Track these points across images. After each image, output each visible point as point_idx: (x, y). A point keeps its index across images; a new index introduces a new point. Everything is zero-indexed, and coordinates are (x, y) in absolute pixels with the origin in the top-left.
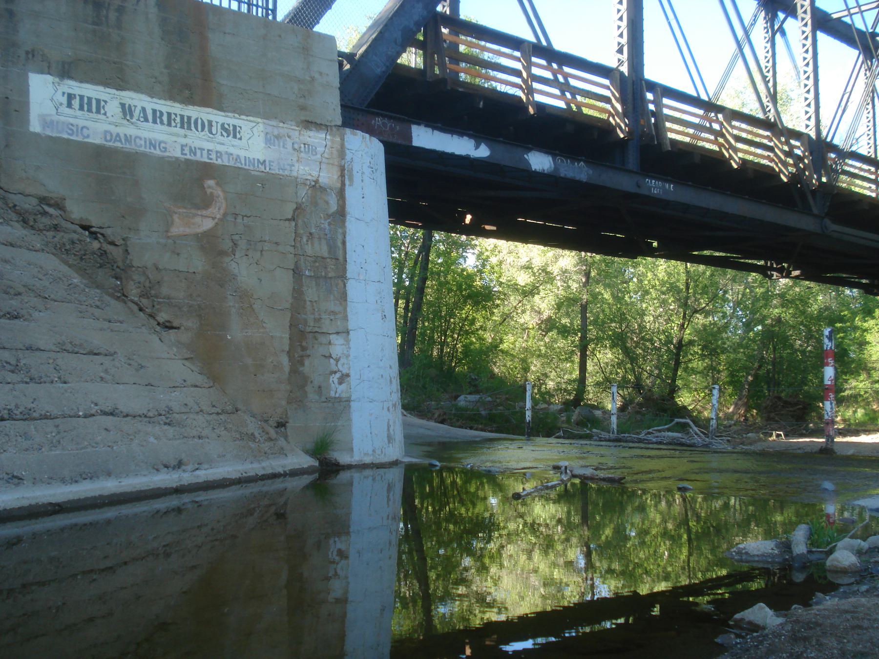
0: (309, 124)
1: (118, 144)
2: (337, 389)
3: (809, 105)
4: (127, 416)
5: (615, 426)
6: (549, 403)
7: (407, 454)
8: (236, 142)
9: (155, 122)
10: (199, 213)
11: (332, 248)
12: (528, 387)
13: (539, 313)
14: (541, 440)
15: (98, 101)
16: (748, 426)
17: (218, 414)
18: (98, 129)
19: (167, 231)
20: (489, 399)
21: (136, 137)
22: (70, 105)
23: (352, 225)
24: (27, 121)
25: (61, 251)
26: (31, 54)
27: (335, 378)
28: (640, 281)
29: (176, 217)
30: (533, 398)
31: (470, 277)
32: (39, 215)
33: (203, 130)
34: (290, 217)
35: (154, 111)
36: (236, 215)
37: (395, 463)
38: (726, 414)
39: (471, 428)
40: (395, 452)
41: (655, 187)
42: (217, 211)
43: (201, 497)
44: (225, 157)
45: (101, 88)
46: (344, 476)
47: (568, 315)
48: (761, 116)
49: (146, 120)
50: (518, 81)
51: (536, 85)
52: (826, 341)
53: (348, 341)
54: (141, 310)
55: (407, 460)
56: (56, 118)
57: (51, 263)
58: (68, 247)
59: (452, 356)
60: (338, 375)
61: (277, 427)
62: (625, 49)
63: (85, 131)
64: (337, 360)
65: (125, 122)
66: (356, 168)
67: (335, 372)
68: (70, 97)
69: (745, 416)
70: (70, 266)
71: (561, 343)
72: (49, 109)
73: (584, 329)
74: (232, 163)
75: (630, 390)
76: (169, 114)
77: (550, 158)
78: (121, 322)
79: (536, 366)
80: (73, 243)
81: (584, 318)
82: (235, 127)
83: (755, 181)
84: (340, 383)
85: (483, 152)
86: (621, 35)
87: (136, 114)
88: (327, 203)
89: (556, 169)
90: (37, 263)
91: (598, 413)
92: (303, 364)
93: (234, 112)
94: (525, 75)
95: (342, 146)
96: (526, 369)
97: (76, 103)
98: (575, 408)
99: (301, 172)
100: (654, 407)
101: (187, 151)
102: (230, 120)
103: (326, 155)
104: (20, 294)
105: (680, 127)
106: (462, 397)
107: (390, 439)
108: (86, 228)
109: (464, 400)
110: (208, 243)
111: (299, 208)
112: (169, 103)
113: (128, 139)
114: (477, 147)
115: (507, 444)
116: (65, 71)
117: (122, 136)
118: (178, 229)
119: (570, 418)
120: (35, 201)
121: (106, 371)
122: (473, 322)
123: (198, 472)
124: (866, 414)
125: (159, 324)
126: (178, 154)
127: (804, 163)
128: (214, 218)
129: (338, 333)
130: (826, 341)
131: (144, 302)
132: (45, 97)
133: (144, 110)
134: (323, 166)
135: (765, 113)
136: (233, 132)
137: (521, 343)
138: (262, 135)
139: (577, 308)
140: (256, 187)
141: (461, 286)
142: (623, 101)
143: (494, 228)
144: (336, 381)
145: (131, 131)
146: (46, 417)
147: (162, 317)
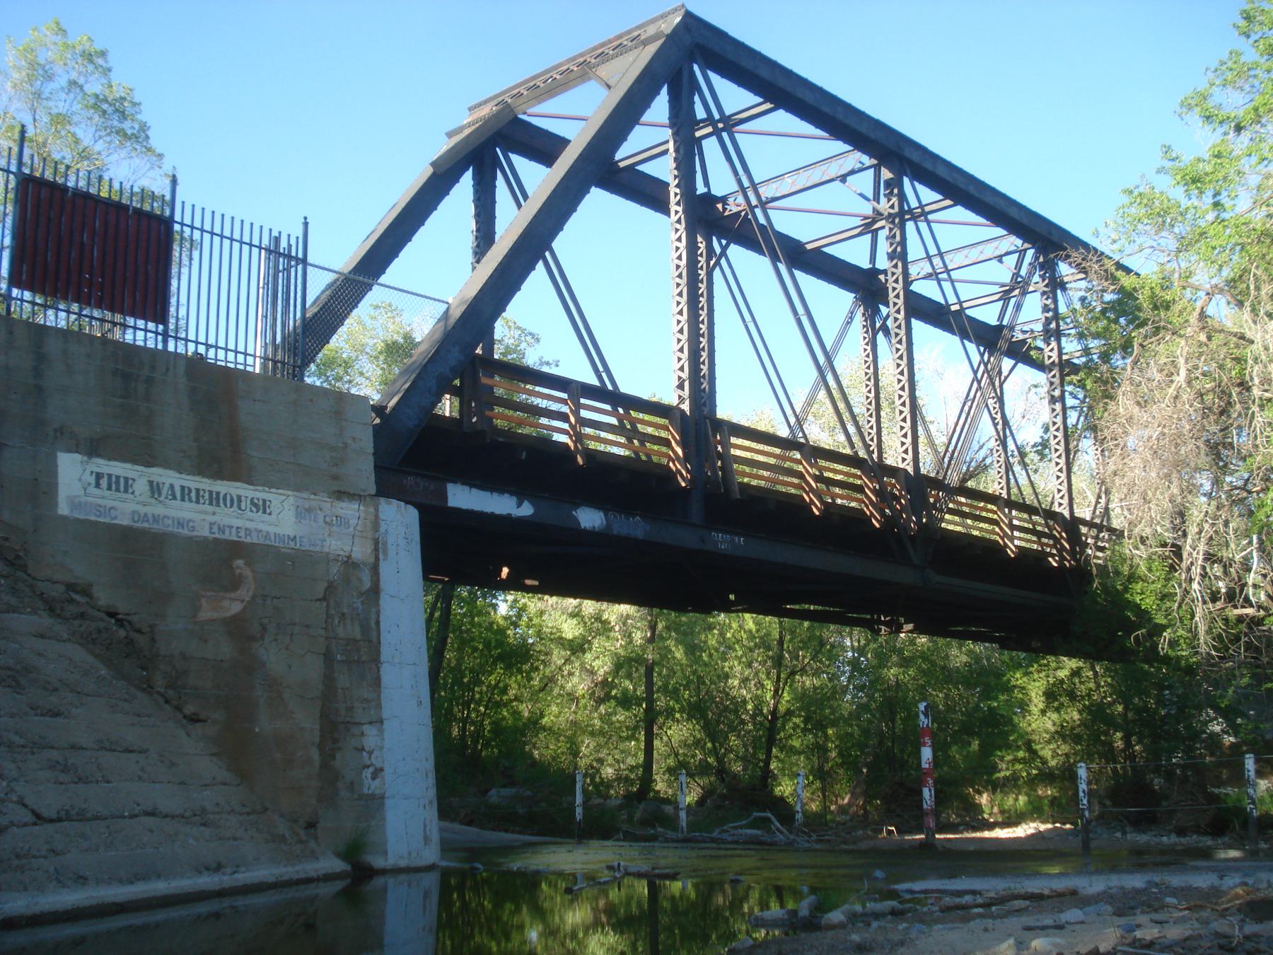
0: (340, 495)
1: (146, 525)
2: (370, 785)
3: (905, 436)
4: (166, 816)
5: (684, 824)
6: (607, 797)
7: (443, 858)
8: (266, 517)
9: (183, 500)
10: (228, 595)
11: (365, 629)
12: (578, 778)
13: (592, 672)
14: (595, 843)
15: (126, 479)
16: (863, 820)
17: (248, 814)
18: (126, 509)
19: (195, 616)
20: (529, 793)
21: (165, 517)
22: (98, 485)
23: (386, 603)
24: (56, 504)
25: (88, 641)
26: (60, 431)
27: (368, 773)
28: (722, 634)
29: (203, 601)
30: (584, 791)
31: (502, 631)
32: (66, 604)
33: (232, 506)
34: (321, 596)
35: (183, 488)
36: (265, 597)
37: (431, 868)
38: (840, 806)
39: (506, 831)
40: (431, 855)
41: (722, 541)
42: (245, 593)
43: (241, 902)
44: (254, 534)
45: (129, 466)
46: (378, 881)
47: (629, 676)
48: (848, 451)
49: (174, 498)
50: (566, 426)
51: (588, 431)
52: (922, 717)
53: (381, 731)
54: (167, 702)
55: (444, 864)
56: (84, 499)
57: (78, 653)
58: (94, 636)
59: (477, 735)
60: (371, 770)
61: (307, 828)
62: (687, 384)
63: (113, 513)
64: (370, 753)
65: (153, 500)
66: (391, 540)
67: (368, 767)
68: (99, 476)
69: (865, 809)
70: (96, 656)
71: (621, 716)
72: (77, 490)
73: (650, 700)
74: (261, 541)
75: (712, 779)
76: (198, 490)
77: (602, 514)
78: (149, 716)
79: (587, 746)
80: (99, 631)
81: (650, 684)
82: (264, 501)
83: (842, 528)
84: (374, 778)
85: (526, 510)
86: (682, 369)
87: (164, 492)
88: (360, 580)
89: (609, 526)
90: (63, 657)
91: (669, 809)
92: (333, 757)
93: (264, 485)
94: (572, 420)
95: (377, 516)
96: (575, 753)
97: (104, 483)
98: (639, 802)
99: (333, 547)
100: (741, 798)
101: (215, 529)
102: (259, 494)
103: (359, 528)
104: (56, 690)
105: (751, 464)
106: (493, 792)
107: (426, 840)
108: (112, 615)
109: (496, 795)
110: (238, 629)
111: (331, 587)
112: (197, 478)
113: (156, 519)
114: (519, 505)
115: (553, 848)
116: (93, 448)
117: (150, 515)
118: (206, 614)
119: (632, 813)
120: (62, 588)
121: (142, 769)
122: (504, 691)
123: (236, 875)
124: (1030, 802)
125: (185, 717)
126: (206, 533)
127: (901, 504)
128: (243, 601)
129: (371, 723)
130: (922, 717)
131: (171, 693)
132: (74, 477)
133: (172, 486)
134: (357, 540)
135: (852, 445)
136: (263, 507)
137: (568, 714)
138: (293, 508)
139: (642, 670)
140: (285, 564)
141: (490, 642)
142: (683, 444)
143: (536, 583)
144: (369, 776)
145: (159, 510)
146: (97, 818)
147: (190, 709)
